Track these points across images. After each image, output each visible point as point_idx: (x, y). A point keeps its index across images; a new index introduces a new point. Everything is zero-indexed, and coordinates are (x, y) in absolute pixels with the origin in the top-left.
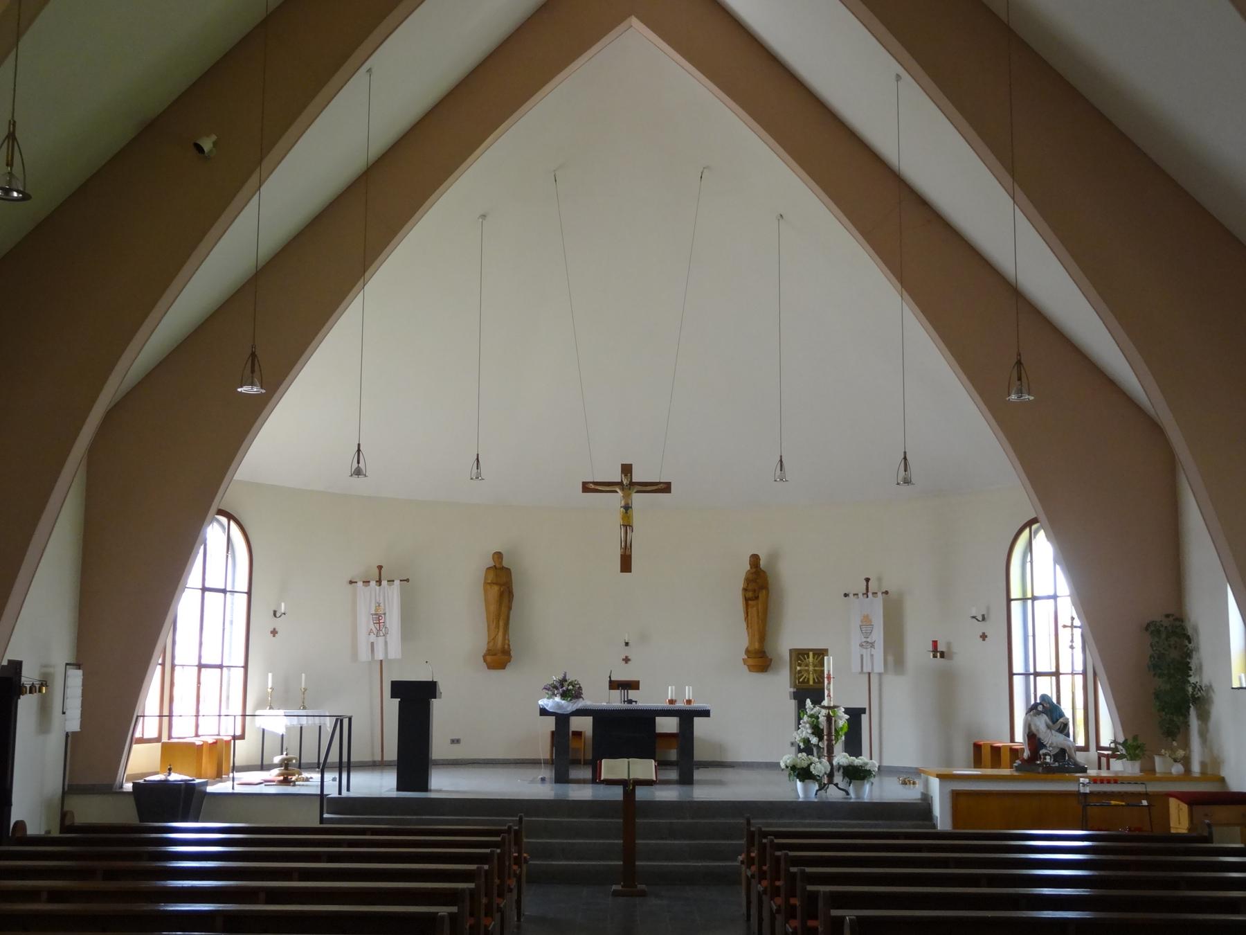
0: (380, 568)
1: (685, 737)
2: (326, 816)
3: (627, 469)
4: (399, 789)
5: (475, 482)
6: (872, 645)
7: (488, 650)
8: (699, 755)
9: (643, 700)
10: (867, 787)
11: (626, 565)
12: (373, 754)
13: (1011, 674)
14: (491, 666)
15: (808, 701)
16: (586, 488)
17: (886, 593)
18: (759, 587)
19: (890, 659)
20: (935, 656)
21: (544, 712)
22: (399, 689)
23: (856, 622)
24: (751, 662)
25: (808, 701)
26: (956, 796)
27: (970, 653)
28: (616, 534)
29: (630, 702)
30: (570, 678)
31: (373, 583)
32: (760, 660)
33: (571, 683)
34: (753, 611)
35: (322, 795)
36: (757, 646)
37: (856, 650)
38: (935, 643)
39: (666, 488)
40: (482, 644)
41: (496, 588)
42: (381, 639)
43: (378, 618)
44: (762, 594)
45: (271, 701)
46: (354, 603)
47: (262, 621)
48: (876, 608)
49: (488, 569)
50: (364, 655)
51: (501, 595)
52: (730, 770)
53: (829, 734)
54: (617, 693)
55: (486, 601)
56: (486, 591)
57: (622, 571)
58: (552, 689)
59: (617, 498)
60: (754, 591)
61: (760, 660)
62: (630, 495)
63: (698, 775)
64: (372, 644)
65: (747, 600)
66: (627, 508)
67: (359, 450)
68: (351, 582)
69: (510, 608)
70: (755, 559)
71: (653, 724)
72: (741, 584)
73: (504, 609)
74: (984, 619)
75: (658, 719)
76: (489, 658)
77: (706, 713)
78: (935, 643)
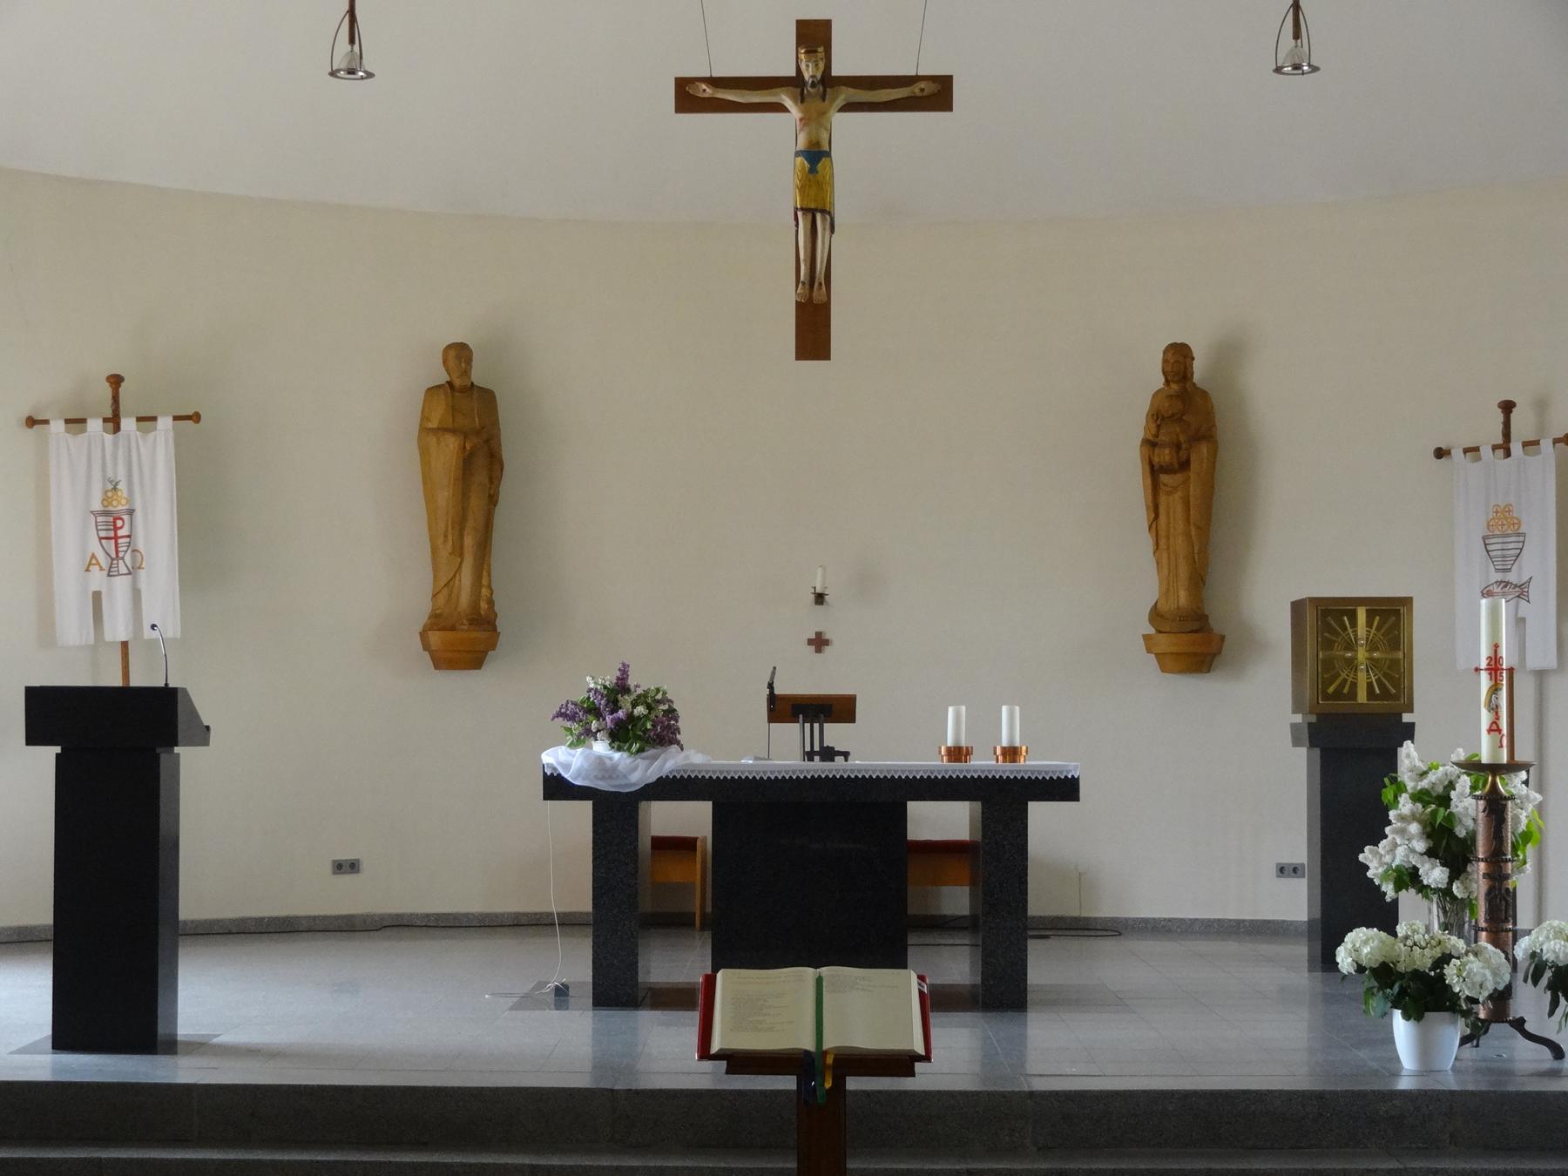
0: (116, 381)
1: (999, 855)
3: (814, 36)
4: (66, 1037)
5: (345, 85)
6: (1521, 591)
8: (1040, 903)
9: (867, 750)
11: (813, 334)
16: (688, 97)
18: (1188, 435)
21: (556, 787)
22: (50, 713)
24: (1166, 643)
29: (828, 754)
30: (640, 681)
31: (95, 425)
32: (1194, 638)
33: (640, 700)
34: (1172, 503)
36: (1183, 598)
39: (933, 94)
40: (418, 603)
42: (121, 584)
43: (113, 525)
49: (432, 391)
51: (467, 463)
52: (1108, 945)
53: (1496, 858)
57: (826, 25)
58: (582, 717)
59: (780, 132)
62: (823, 113)
63: (1045, 966)
64: (97, 596)
65: (1155, 471)
66: (816, 155)
68: (32, 422)
69: (493, 500)
70: (1178, 359)
71: (900, 819)
72: (1135, 426)
73: (476, 503)
75: (912, 806)
76: (435, 638)
77: (1064, 789)
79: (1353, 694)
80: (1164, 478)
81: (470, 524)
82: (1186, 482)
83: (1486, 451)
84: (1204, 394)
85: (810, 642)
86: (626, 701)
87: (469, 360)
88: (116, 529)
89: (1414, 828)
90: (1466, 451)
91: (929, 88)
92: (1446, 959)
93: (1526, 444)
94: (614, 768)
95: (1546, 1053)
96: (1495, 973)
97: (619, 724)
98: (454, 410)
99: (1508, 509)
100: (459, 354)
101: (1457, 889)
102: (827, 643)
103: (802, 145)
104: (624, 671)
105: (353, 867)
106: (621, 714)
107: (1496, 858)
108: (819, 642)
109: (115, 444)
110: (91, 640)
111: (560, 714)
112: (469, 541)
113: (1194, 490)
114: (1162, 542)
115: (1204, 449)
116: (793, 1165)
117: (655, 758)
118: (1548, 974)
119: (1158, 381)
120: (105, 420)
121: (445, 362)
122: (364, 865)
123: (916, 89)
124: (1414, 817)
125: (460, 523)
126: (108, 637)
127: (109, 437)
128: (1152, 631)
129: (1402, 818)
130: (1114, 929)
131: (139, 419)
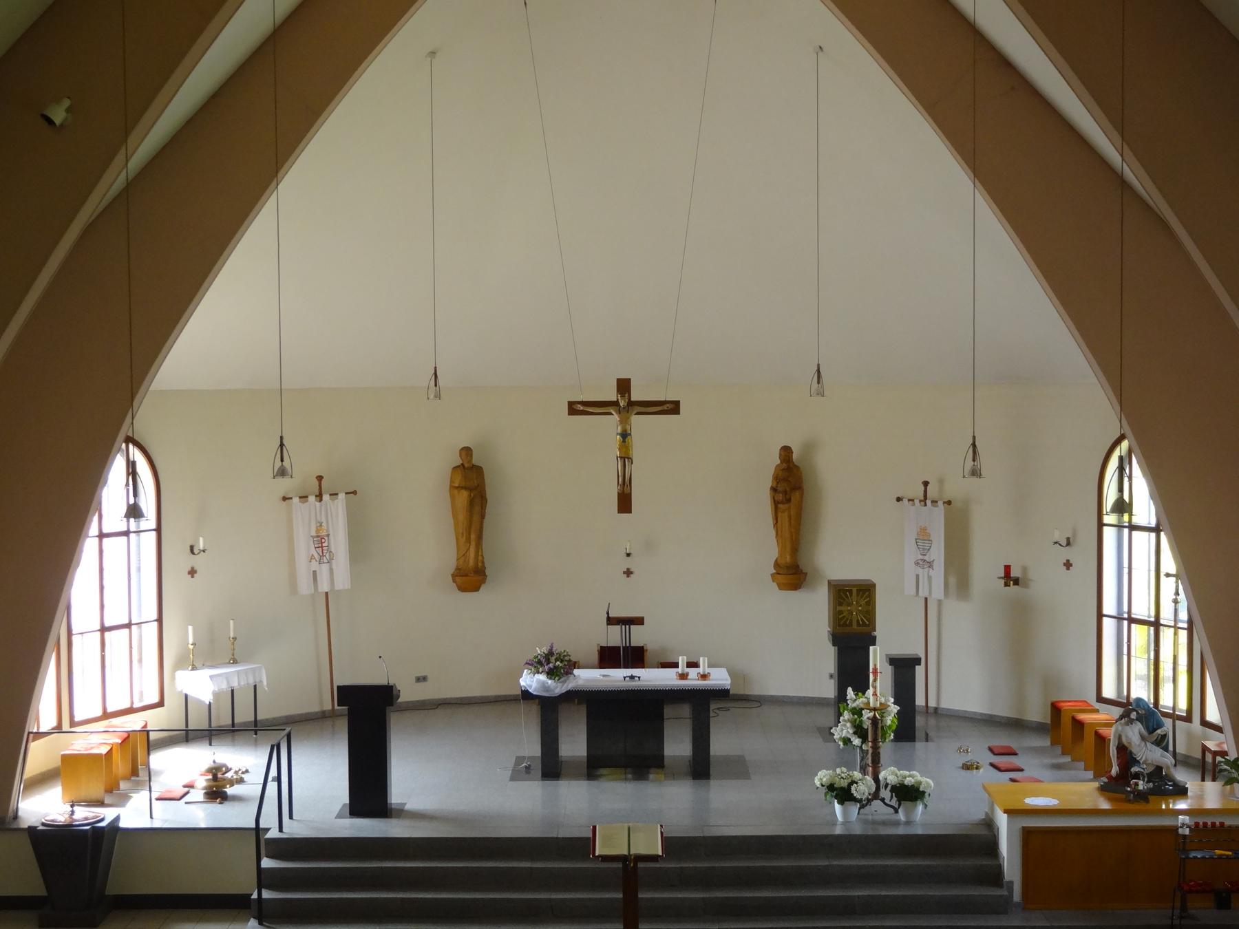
0: (320, 478)
2: (266, 863)
3: (624, 386)
7: (458, 569)
10: (920, 808)
11: (625, 503)
12: (321, 703)
13: (1100, 616)
14: (463, 588)
15: (850, 690)
16: (574, 409)
17: (949, 503)
18: (791, 486)
19: (953, 581)
20: (1006, 585)
24: (781, 578)
25: (850, 690)
26: (1027, 834)
27: (1046, 578)
30: (558, 648)
31: (312, 499)
32: (793, 574)
35: (258, 831)
36: (788, 559)
37: (910, 570)
38: (1007, 569)
39: (673, 408)
40: (451, 562)
41: (465, 493)
42: (325, 567)
43: (321, 541)
44: (796, 496)
45: (192, 661)
46: (290, 521)
47: (177, 561)
48: (936, 519)
50: (305, 586)
51: (471, 503)
56: (452, 497)
57: (628, 381)
58: (537, 664)
59: (611, 422)
60: (785, 492)
61: (793, 574)
64: (315, 572)
65: (776, 503)
66: (625, 435)
67: (282, 445)
68: (285, 499)
69: (483, 517)
70: (786, 451)
72: (768, 482)
73: (476, 518)
74: (1068, 544)
76: (458, 579)
78: (1007, 569)
79: (851, 624)
82: (789, 508)
83: (917, 502)
84: (797, 467)
89: (848, 725)
92: (853, 782)
95: (892, 810)
100: (467, 451)
101: (864, 747)
105: (424, 679)
107: (875, 741)
108: (628, 573)
112: (473, 536)
113: (793, 512)
115: (797, 493)
117: (564, 682)
123: (665, 407)
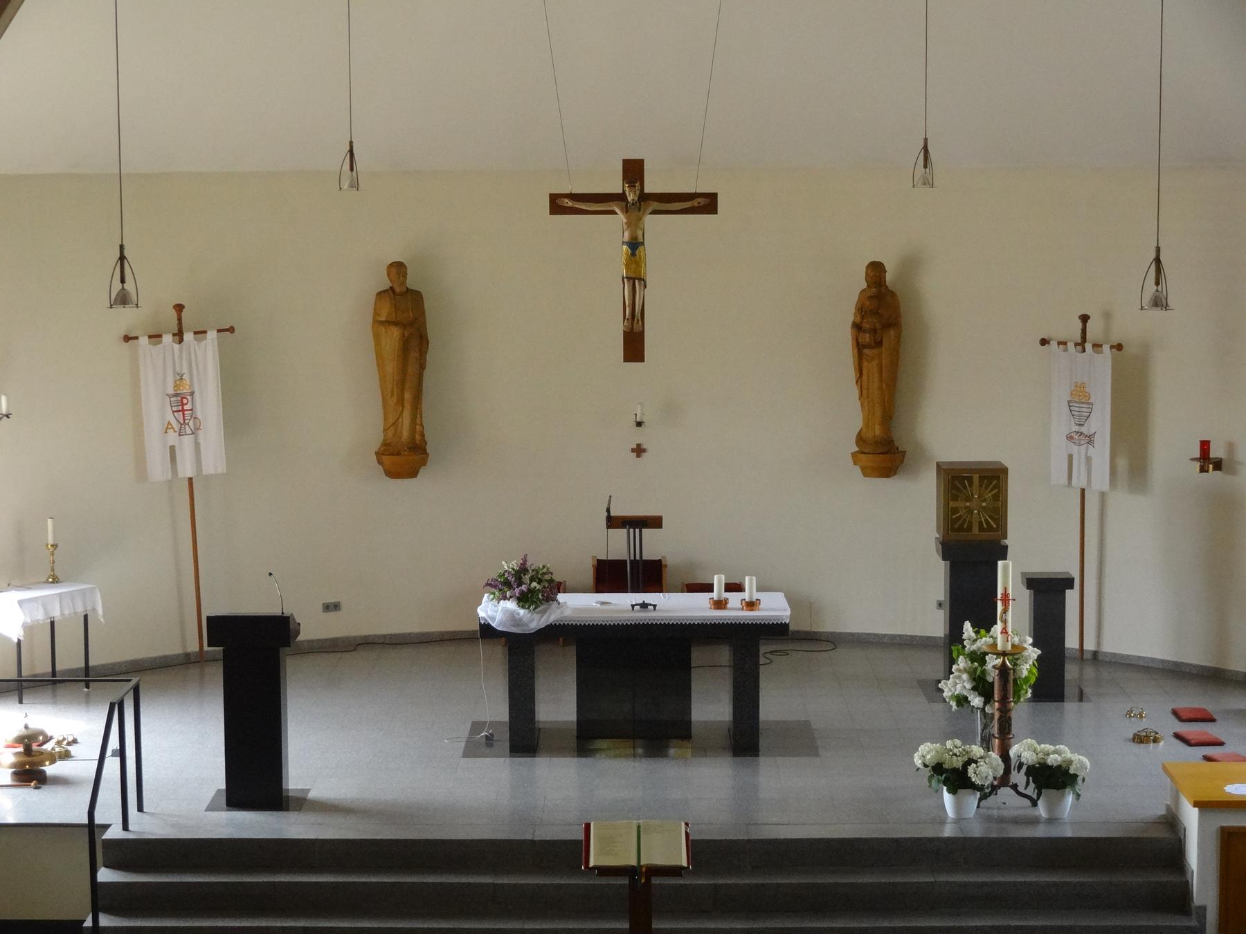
0: (179, 308)
2: (105, 875)
3: (633, 171)
6: (1090, 439)
7: (385, 444)
10: (1070, 798)
11: (634, 347)
14: (393, 473)
17: (1119, 347)
18: (883, 322)
19: (1122, 463)
20: (1203, 470)
23: (1061, 395)
25: (967, 626)
28: (654, 299)
30: (534, 563)
31: (167, 338)
32: (884, 453)
35: (92, 829)
36: (878, 431)
38: (1205, 445)
40: (374, 436)
41: (395, 332)
42: (188, 441)
43: (181, 402)
48: (1101, 368)
50: (158, 468)
54: (621, 534)
55: (380, 357)
58: (502, 586)
59: (615, 225)
60: (874, 331)
61: (884, 453)
64: (172, 448)
65: (860, 347)
66: (635, 245)
67: (122, 258)
68: (127, 338)
69: (422, 367)
70: (876, 270)
72: (848, 314)
73: (412, 369)
76: (387, 459)
78: (1205, 445)
79: (970, 529)
80: (866, 351)
81: (407, 385)
83: (1071, 345)
84: (893, 294)
85: (633, 450)
86: (526, 578)
87: (405, 275)
88: (183, 405)
89: (965, 676)
90: (1059, 343)
91: (702, 201)
93: (1094, 346)
94: (520, 620)
96: (995, 770)
97: (522, 593)
98: (396, 307)
99: (1083, 386)
100: (398, 268)
102: (644, 451)
103: (626, 238)
104: (525, 560)
106: (524, 587)
107: (1004, 700)
108: (639, 451)
109: (181, 350)
110: (169, 476)
111: (488, 584)
112: (408, 396)
114: (865, 391)
116: (627, 926)
117: (544, 612)
118: (1024, 768)
119: (865, 285)
120: (174, 335)
121: (388, 275)
122: (343, 605)
123: (695, 203)
124: (965, 670)
125: (402, 384)
126: (181, 475)
127: (176, 346)
128: (857, 449)
129: (959, 671)
130: (834, 641)
131: (196, 333)
